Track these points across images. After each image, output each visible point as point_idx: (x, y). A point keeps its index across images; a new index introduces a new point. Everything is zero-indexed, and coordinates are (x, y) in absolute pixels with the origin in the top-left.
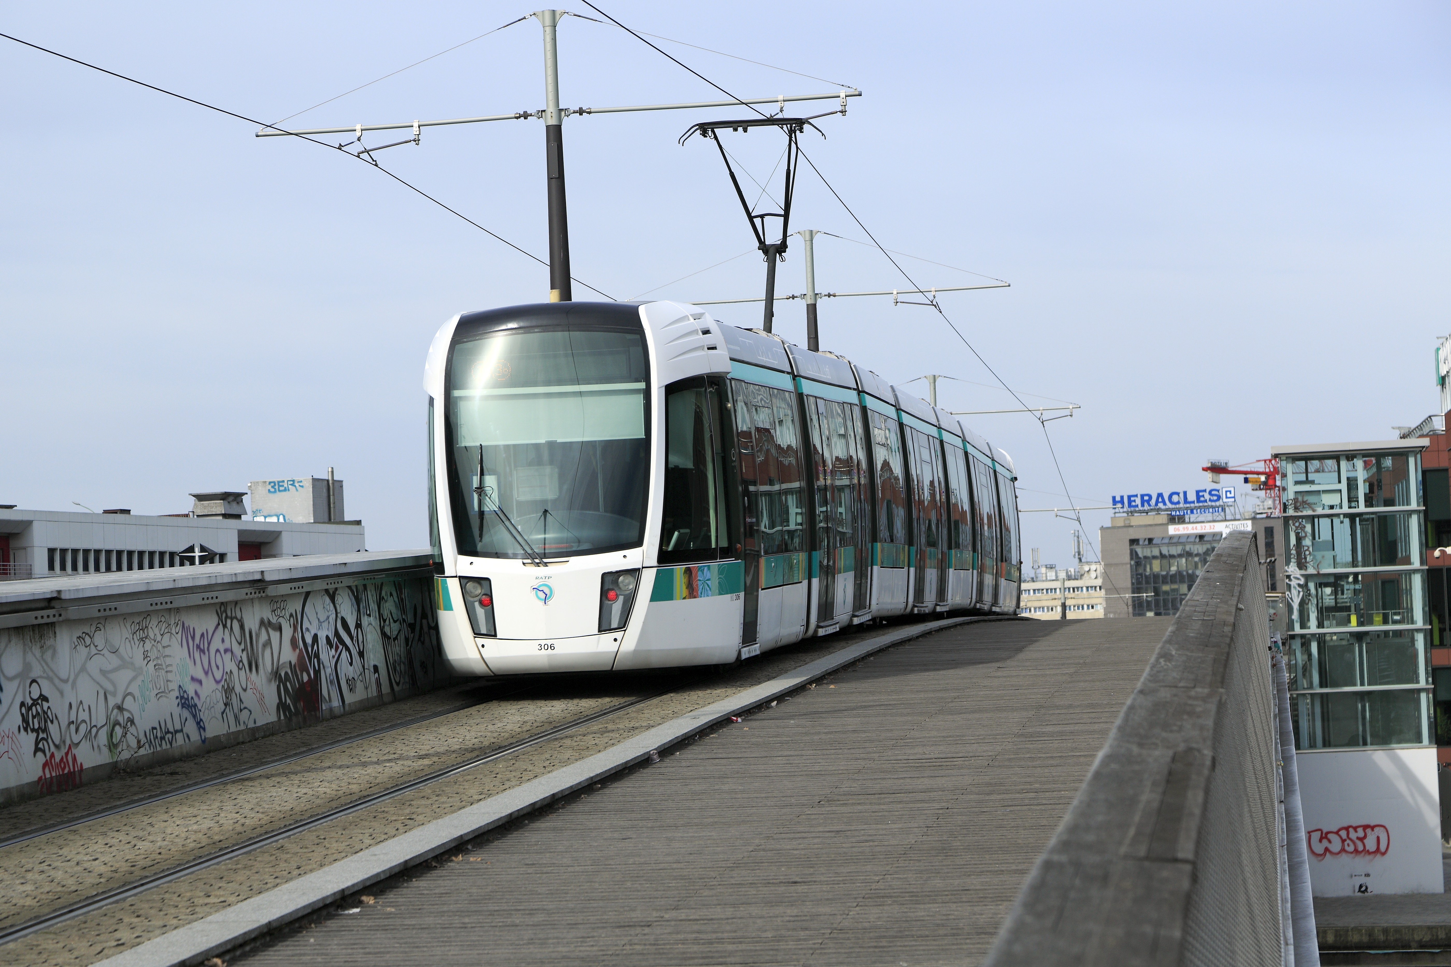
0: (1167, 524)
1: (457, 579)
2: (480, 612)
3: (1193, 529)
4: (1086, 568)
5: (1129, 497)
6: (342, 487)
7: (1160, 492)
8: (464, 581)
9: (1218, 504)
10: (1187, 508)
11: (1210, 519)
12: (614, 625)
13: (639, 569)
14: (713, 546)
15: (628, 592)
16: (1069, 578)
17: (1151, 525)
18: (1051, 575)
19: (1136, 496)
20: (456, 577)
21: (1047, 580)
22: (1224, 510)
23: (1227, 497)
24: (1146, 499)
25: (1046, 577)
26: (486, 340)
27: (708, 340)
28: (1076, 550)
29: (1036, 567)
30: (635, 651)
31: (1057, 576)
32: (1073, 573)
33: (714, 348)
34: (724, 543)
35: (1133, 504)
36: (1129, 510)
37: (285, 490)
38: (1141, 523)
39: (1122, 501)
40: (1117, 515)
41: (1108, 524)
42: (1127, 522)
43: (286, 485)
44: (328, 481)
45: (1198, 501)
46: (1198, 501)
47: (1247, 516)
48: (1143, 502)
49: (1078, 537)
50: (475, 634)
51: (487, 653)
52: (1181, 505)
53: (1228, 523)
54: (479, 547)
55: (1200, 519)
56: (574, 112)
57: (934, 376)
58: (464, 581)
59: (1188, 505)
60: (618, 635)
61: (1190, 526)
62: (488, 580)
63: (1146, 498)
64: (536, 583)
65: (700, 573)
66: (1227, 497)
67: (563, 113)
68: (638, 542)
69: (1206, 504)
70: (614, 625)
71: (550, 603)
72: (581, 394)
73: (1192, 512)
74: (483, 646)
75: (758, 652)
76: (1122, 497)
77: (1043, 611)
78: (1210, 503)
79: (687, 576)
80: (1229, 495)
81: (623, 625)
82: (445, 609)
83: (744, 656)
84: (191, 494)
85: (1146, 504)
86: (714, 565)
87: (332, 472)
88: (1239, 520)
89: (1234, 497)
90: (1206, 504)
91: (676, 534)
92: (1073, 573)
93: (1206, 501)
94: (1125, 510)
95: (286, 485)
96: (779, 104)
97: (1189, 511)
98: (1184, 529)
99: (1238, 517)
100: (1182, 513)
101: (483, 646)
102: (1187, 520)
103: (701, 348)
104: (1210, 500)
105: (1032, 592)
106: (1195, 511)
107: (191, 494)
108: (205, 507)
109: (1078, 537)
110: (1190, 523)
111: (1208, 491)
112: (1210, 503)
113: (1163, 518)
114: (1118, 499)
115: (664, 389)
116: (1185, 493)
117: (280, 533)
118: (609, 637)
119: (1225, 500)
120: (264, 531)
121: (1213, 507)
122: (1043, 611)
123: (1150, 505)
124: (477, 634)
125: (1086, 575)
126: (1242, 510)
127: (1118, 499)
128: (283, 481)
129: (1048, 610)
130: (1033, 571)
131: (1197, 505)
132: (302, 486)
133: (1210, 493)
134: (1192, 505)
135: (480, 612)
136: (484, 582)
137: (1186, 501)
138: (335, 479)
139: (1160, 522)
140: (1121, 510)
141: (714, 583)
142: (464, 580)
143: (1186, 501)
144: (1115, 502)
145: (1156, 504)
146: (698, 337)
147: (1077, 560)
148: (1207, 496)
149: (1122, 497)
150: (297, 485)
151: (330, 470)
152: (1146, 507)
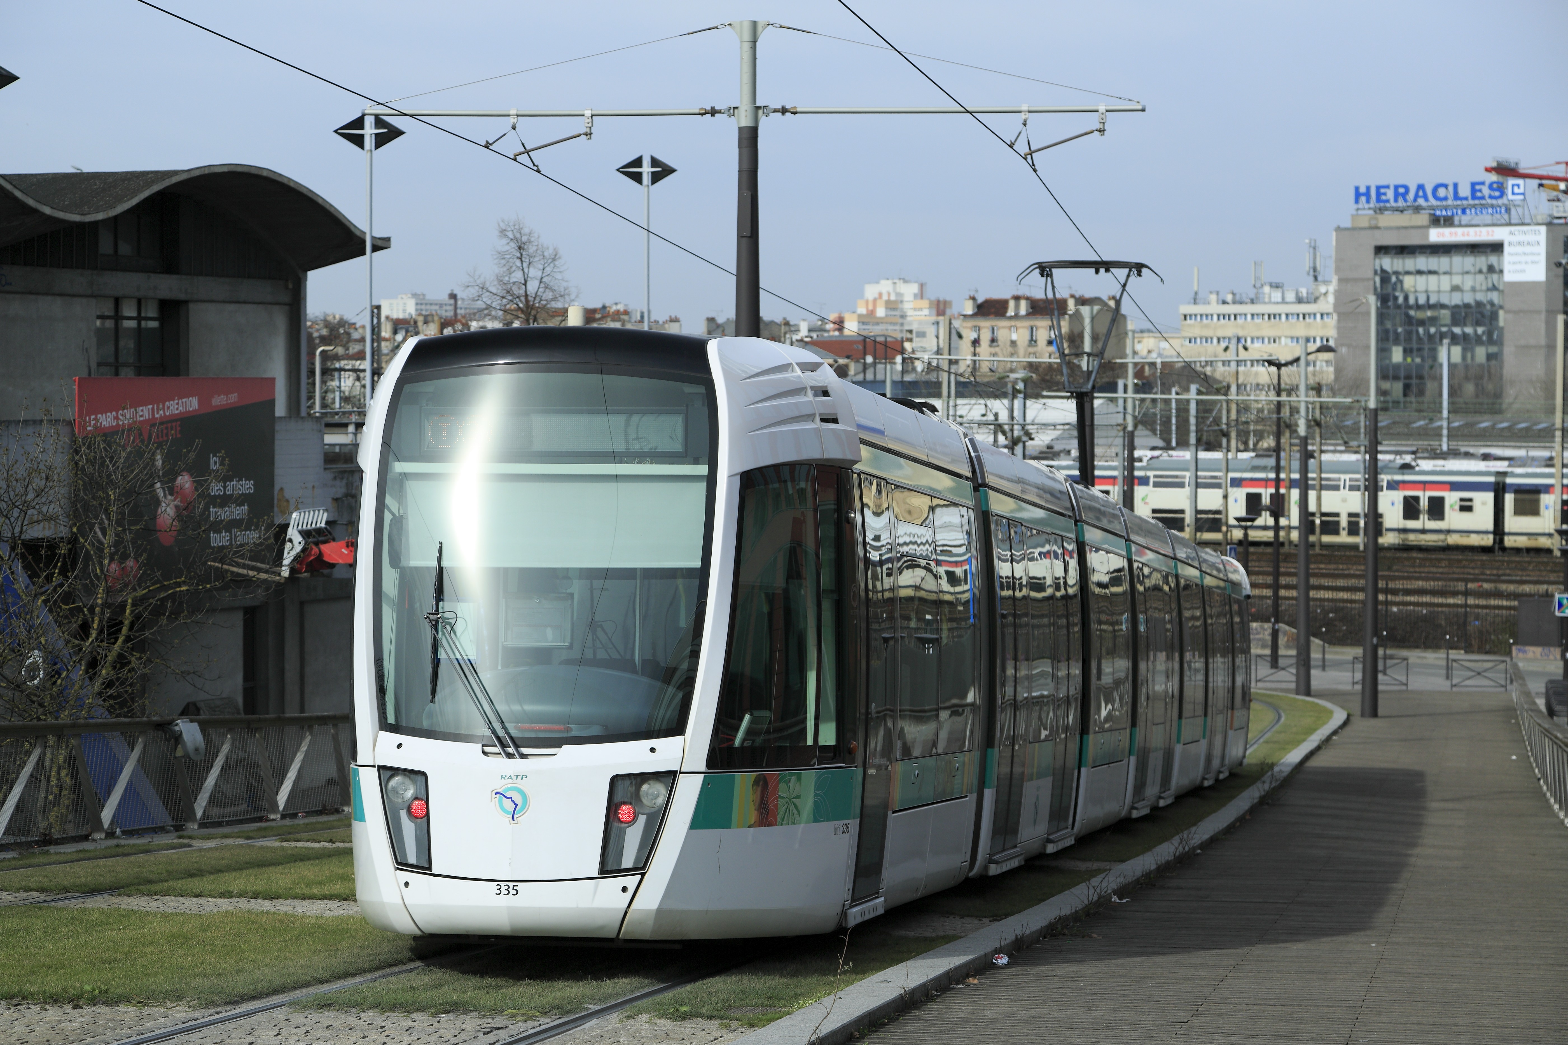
0: (1428, 227)
1: (376, 769)
2: (408, 828)
3: (1463, 235)
4: (1323, 289)
5: (1378, 188)
7: (1421, 182)
8: (386, 774)
9: (1500, 202)
10: (1456, 207)
11: (1489, 222)
12: (628, 862)
13: (674, 773)
14: (810, 742)
15: (653, 810)
16: (1300, 300)
17: (1406, 228)
18: (1277, 296)
19: (1388, 187)
20: (374, 766)
21: (1270, 302)
22: (1508, 210)
23: (1513, 194)
24: (1401, 191)
25: (1270, 297)
28: (1312, 265)
29: (1258, 285)
30: (659, 912)
31: (1283, 298)
32: (1305, 295)
33: (835, 421)
35: (1383, 198)
36: (1378, 205)
38: (1393, 224)
39: (1367, 194)
40: (1360, 212)
41: (1347, 224)
42: (1373, 223)
45: (1474, 197)
46: (1474, 197)
47: (1540, 219)
48: (1397, 195)
49: (1315, 248)
50: (398, 863)
52: (1450, 202)
53: (1512, 228)
55: (1474, 222)
56: (775, 111)
57: (754, 24)
58: (386, 774)
59: (1459, 202)
60: (631, 881)
61: (1460, 230)
62: (423, 774)
63: (1401, 190)
64: (500, 785)
65: (782, 786)
66: (1513, 194)
67: (760, 112)
68: (677, 727)
69: (1483, 202)
70: (628, 862)
71: (523, 819)
73: (1464, 211)
75: (881, 911)
76: (1368, 188)
77: (1263, 342)
78: (1489, 201)
80: (1516, 190)
81: (640, 868)
82: (355, 820)
83: (852, 922)
85: (1400, 199)
86: (809, 777)
88: (1528, 224)
89: (1523, 194)
90: (1483, 202)
91: (747, 717)
92: (1305, 295)
93: (1483, 198)
94: (1372, 205)
96: (1023, 116)
97: (1460, 212)
98: (1451, 234)
99: (1527, 221)
100: (1449, 213)
102: (1456, 222)
104: (1491, 197)
105: (1249, 317)
106: (1468, 211)
109: (1315, 248)
110: (1460, 225)
111: (1487, 183)
112: (1489, 201)
113: (1423, 219)
114: (1363, 190)
115: (739, 477)
116: (1456, 186)
119: (1511, 197)
121: (1492, 206)
122: (1263, 342)
123: (1406, 200)
124: (402, 864)
125: (1322, 298)
126: (1533, 212)
127: (1363, 190)
129: (1269, 342)
130: (1255, 291)
131: (1471, 202)
133: (1491, 187)
134: (1465, 202)
136: (419, 776)
137: (1456, 197)
139: (1419, 223)
140: (1367, 206)
141: (807, 805)
142: (387, 772)
143: (1456, 197)
144: (1358, 195)
145: (1415, 200)
146: (805, 399)
147: (1311, 278)
148: (1486, 191)
149: (1368, 188)
152: (1401, 203)
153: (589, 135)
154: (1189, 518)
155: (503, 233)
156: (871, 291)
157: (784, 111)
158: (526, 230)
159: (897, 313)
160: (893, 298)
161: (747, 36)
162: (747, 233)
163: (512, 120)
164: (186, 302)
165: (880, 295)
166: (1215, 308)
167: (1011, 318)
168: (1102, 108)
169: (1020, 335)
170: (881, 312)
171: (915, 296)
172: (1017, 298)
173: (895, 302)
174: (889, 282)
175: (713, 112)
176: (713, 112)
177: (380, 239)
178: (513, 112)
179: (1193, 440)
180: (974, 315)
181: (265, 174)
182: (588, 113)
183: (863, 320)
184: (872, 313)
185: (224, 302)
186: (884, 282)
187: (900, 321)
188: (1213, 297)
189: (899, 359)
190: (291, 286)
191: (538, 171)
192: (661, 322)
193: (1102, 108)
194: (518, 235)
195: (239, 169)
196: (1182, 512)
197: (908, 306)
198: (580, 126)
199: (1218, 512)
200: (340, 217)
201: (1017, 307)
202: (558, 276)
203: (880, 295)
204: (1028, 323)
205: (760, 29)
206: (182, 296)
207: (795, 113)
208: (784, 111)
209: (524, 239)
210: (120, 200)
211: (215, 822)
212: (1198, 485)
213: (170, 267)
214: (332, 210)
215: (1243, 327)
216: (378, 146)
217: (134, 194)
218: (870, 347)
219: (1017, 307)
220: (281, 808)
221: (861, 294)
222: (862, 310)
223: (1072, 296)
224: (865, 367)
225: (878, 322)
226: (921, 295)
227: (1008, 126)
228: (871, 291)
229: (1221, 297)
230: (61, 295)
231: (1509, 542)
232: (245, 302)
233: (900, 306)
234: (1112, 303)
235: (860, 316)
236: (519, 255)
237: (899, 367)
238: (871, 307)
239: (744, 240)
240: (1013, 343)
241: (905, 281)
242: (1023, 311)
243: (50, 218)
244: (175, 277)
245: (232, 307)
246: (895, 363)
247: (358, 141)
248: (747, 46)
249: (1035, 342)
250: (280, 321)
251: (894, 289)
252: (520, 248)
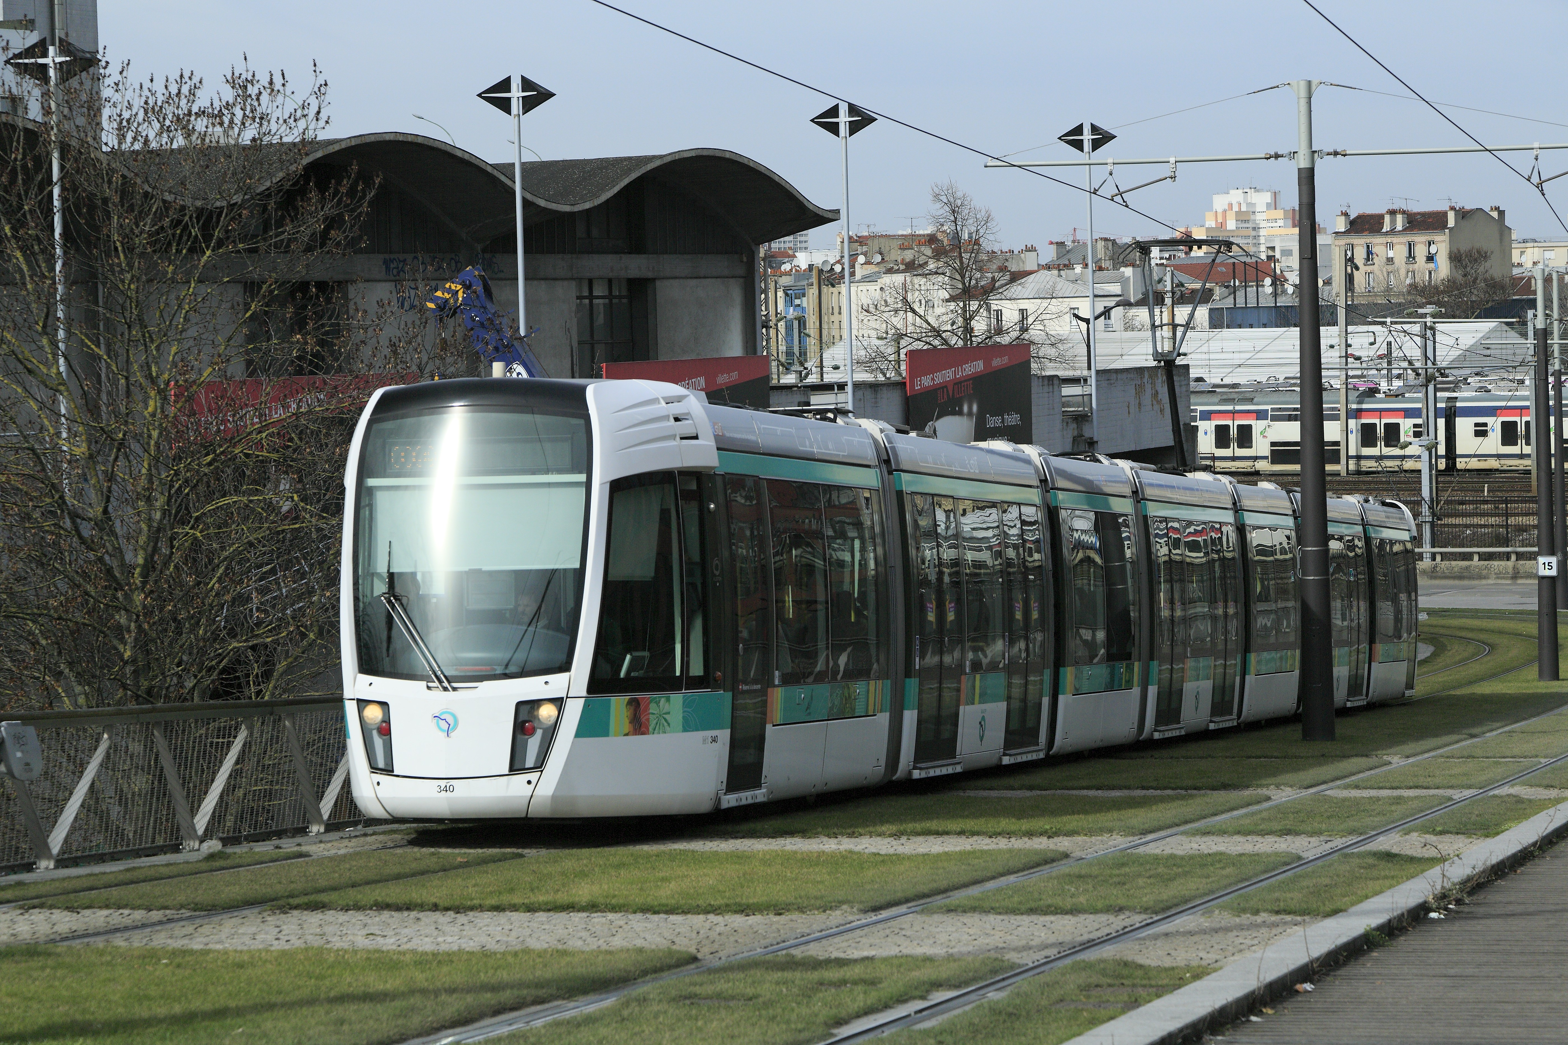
2: (378, 742)
26: (445, 416)
27: (685, 427)
30: (554, 797)
33: (696, 437)
34: (697, 669)
50: (372, 767)
51: (382, 792)
54: (420, 660)
56: (1328, 154)
60: (534, 776)
67: (1316, 155)
68: (565, 666)
70: (530, 763)
72: (549, 485)
74: (378, 783)
79: (632, 708)
81: (539, 766)
91: (628, 657)
96: (1535, 152)
101: (378, 783)
103: (673, 437)
118: (522, 778)
124: (374, 768)
135: (378, 742)
153: (1173, 178)
155: (937, 197)
156: (1220, 202)
157: (1336, 153)
158: (959, 194)
160: (1244, 209)
161: (1303, 93)
162: (1308, 255)
167: (1387, 233)
169: (1399, 253)
170: (1231, 225)
171: (1268, 205)
172: (1393, 213)
174: (1240, 191)
175: (1277, 156)
176: (1277, 156)
177: (830, 211)
178: (1110, 161)
181: (728, 156)
182: (1172, 160)
185: (686, 278)
186: (1233, 192)
187: (1253, 233)
189: (1268, 281)
190: (745, 259)
191: (1127, 206)
192: (1016, 252)
194: (952, 200)
195: (705, 153)
198: (1166, 170)
200: (795, 193)
201: (1393, 222)
202: (991, 237)
204: (1405, 239)
205: (1314, 87)
206: (650, 275)
207: (1345, 155)
208: (1336, 153)
209: (959, 202)
213: (637, 247)
214: (787, 187)
220: (326, 817)
221: (1210, 207)
223: (1452, 208)
226: (1274, 204)
227: (1523, 161)
228: (1220, 202)
230: (546, 279)
232: (705, 277)
233: (1252, 217)
234: (1495, 214)
236: (952, 218)
237: (1269, 290)
238: (1220, 220)
239: (1305, 262)
240: (1390, 260)
243: (545, 209)
244: (644, 256)
245: (693, 282)
246: (1263, 286)
247: (833, 129)
248: (1303, 102)
249: (1414, 258)
250: (737, 294)
251: (1245, 199)
252: (954, 211)
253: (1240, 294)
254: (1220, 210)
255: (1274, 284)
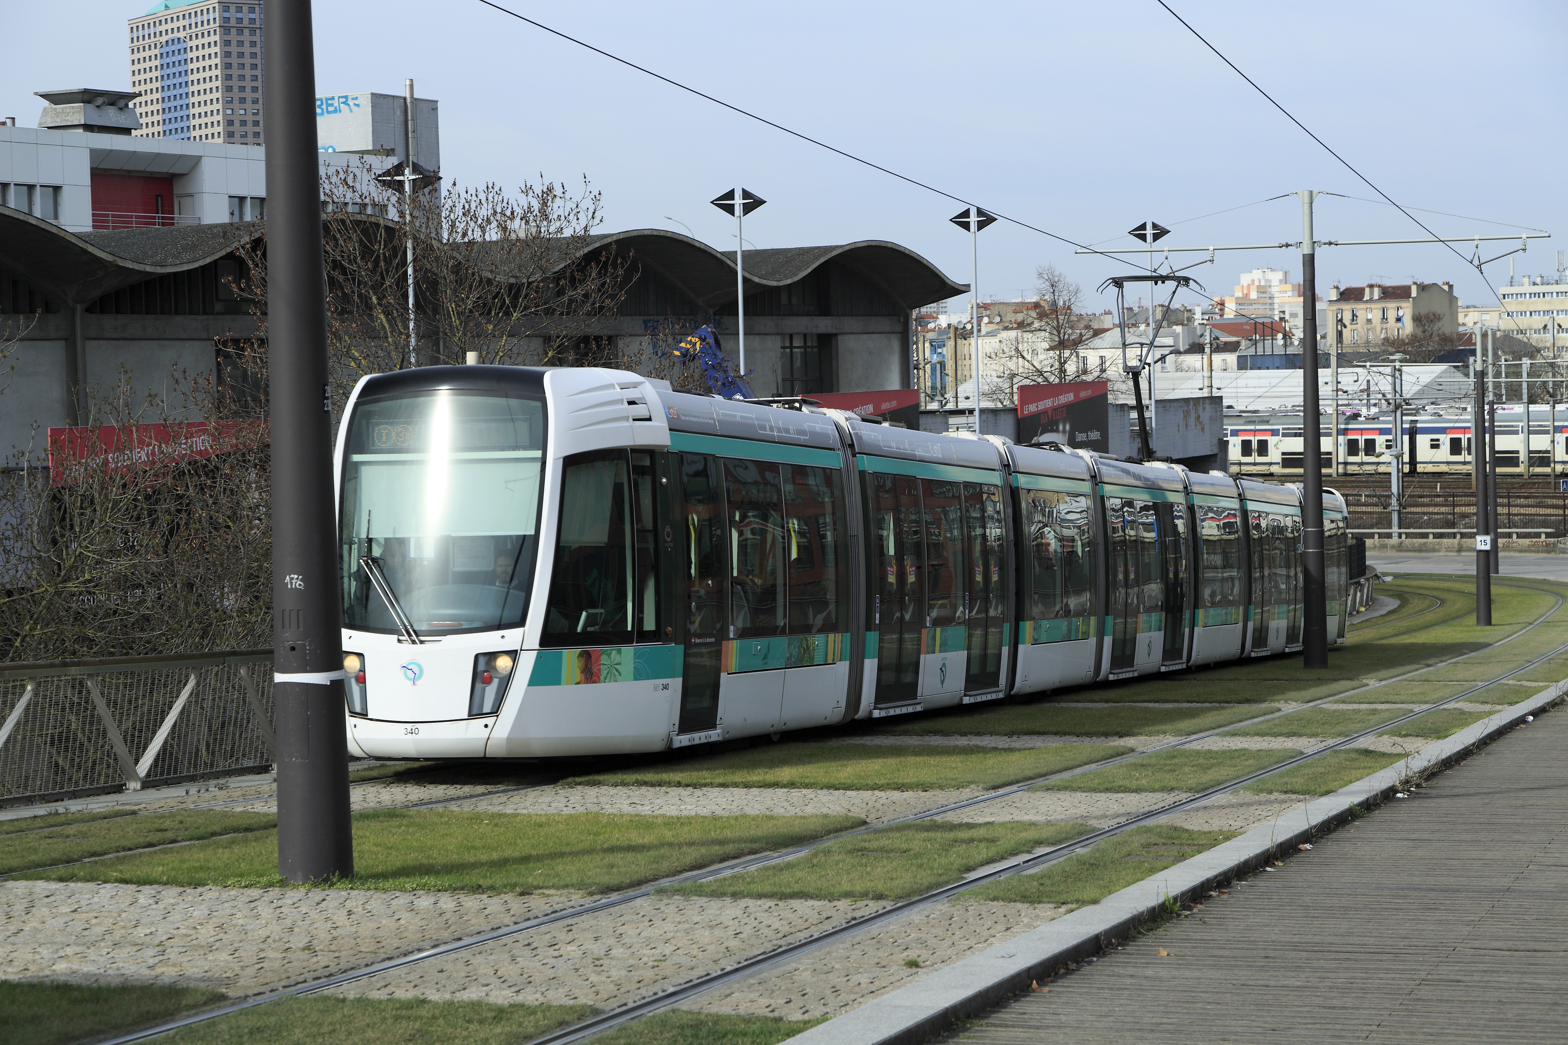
6: (435, 109)
37: (335, 111)
43: (336, 104)
44: (405, 99)
57: (1311, 192)
60: (490, 721)
81: (495, 711)
84: (36, 94)
87: (412, 86)
91: (584, 614)
95: (336, 104)
96: (1476, 242)
107: (36, 94)
108: (57, 114)
117: (199, 158)
120: (134, 153)
128: (333, 98)
132: (358, 105)
138: (415, 96)
150: (351, 103)
151: (408, 82)
154: (1523, 456)
155: (1040, 275)
157: (1330, 243)
158: (1057, 273)
159: (1267, 295)
160: (1263, 283)
161: (1307, 200)
162: (1310, 317)
163: (1165, 254)
164: (836, 335)
165: (1253, 281)
166: (1528, 289)
168: (1524, 236)
169: (1375, 315)
170: (1254, 295)
171: (1281, 281)
172: (1371, 286)
173: (1265, 287)
175: (1287, 245)
176: (1287, 245)
178: (1166, 249)
179: (1525, 397)
180: (1338, 300)
182: (1211, 248)
183: (1240, 302)
184: (1247, 295)
186: (1255, 271)
188: (1526, 280)
189: (1280, 336)
193: (1524, 236)
196: (1518, 452)
197: (1275, 290)
198: (1206, 256)
199: (1548, 452)
201: (1372, 293)
203: (1253, 281)
206: (834, 331)
208: (1330, 243)
209: (1056, 279)
210: (800, 270)
211: (248, 768)
212: (1529, 433)
213: (824, 311)
215: (1550, 303)
216: (979, 229)
217: (808, 265)
218: (1260, 327)
219: (1372, 293)
221: (1238, 282)
222: (1239, 294)
223: (1415, 283)
224: (1256, 343)
225: (1252, 303)
228: (1245, 279)
229: (1532, 280)
230: (759, 334)
231: (1420, 468)
234: (1446, 288)
235: (1237, 299)
240: (1369, 321)
241: (1272, 270)
242: (1376, 297)
243: (758, 284)
245: (865, 336)
248: (1307, 206)
250: (896, 345)
253: (1260, 345)
254: (1245, 284)
255: (1284, 338)
